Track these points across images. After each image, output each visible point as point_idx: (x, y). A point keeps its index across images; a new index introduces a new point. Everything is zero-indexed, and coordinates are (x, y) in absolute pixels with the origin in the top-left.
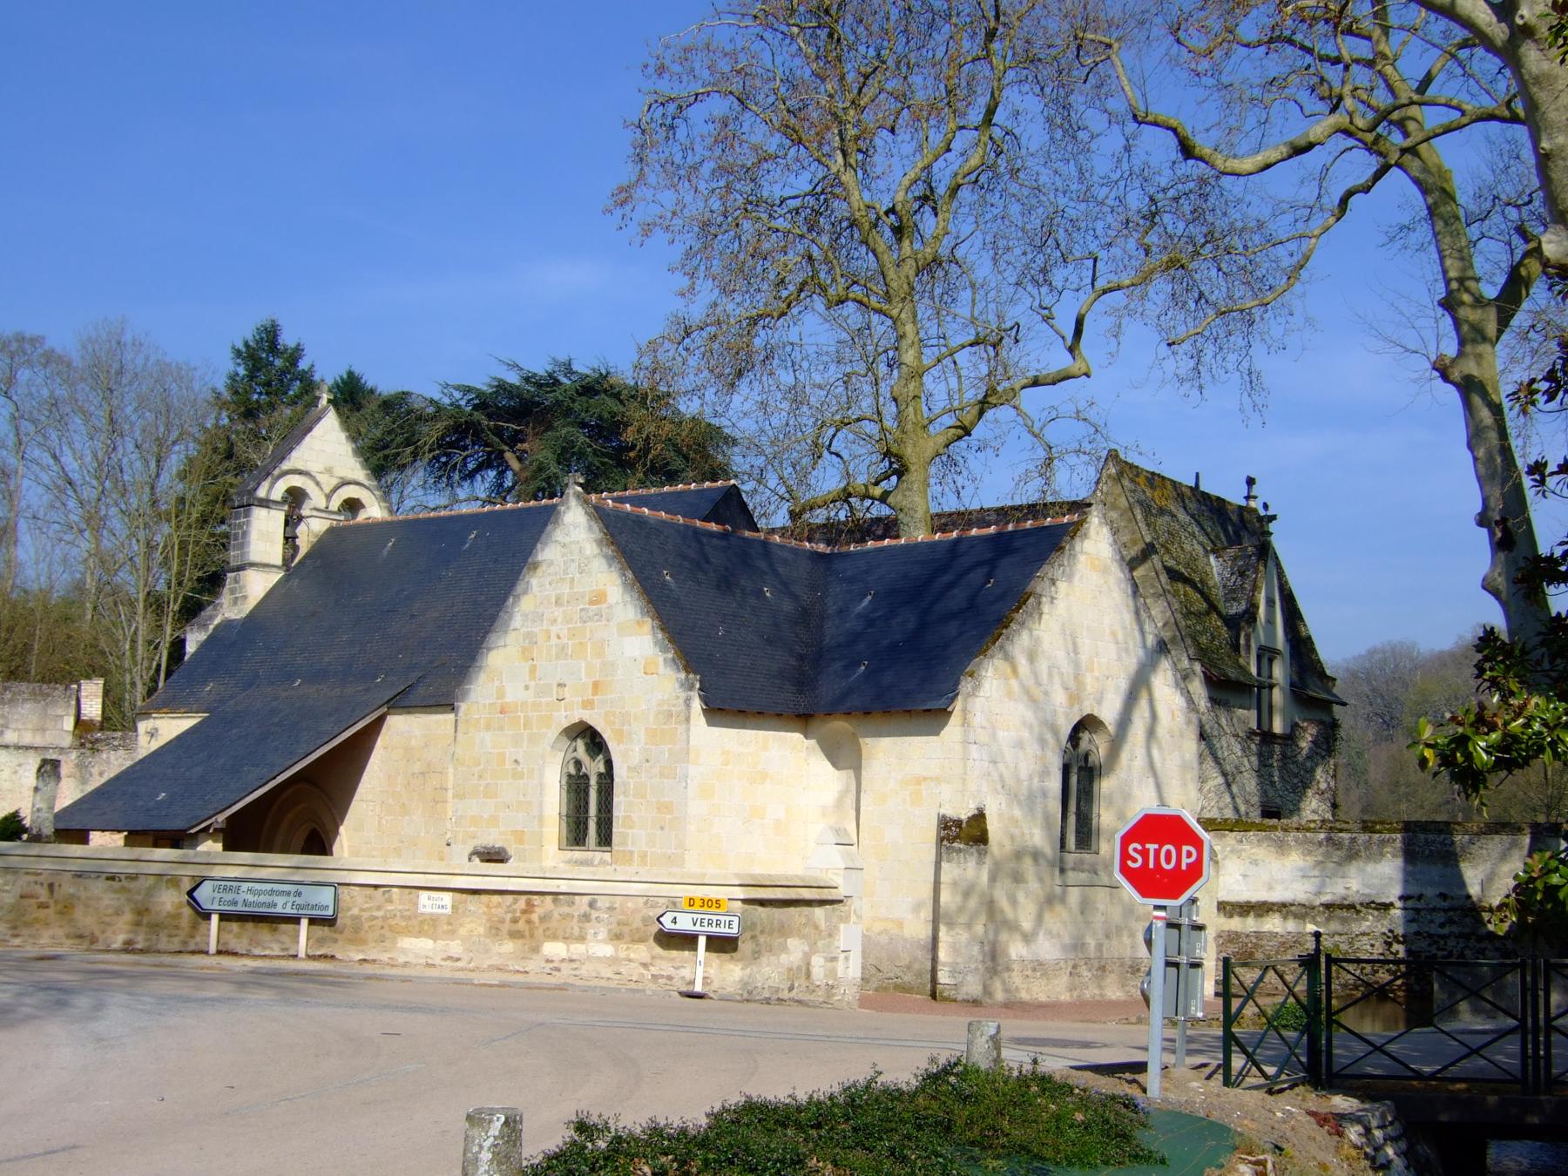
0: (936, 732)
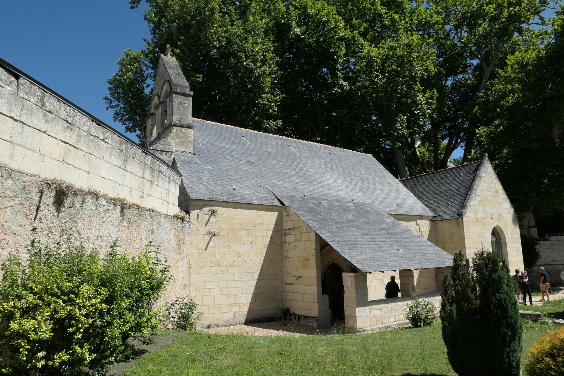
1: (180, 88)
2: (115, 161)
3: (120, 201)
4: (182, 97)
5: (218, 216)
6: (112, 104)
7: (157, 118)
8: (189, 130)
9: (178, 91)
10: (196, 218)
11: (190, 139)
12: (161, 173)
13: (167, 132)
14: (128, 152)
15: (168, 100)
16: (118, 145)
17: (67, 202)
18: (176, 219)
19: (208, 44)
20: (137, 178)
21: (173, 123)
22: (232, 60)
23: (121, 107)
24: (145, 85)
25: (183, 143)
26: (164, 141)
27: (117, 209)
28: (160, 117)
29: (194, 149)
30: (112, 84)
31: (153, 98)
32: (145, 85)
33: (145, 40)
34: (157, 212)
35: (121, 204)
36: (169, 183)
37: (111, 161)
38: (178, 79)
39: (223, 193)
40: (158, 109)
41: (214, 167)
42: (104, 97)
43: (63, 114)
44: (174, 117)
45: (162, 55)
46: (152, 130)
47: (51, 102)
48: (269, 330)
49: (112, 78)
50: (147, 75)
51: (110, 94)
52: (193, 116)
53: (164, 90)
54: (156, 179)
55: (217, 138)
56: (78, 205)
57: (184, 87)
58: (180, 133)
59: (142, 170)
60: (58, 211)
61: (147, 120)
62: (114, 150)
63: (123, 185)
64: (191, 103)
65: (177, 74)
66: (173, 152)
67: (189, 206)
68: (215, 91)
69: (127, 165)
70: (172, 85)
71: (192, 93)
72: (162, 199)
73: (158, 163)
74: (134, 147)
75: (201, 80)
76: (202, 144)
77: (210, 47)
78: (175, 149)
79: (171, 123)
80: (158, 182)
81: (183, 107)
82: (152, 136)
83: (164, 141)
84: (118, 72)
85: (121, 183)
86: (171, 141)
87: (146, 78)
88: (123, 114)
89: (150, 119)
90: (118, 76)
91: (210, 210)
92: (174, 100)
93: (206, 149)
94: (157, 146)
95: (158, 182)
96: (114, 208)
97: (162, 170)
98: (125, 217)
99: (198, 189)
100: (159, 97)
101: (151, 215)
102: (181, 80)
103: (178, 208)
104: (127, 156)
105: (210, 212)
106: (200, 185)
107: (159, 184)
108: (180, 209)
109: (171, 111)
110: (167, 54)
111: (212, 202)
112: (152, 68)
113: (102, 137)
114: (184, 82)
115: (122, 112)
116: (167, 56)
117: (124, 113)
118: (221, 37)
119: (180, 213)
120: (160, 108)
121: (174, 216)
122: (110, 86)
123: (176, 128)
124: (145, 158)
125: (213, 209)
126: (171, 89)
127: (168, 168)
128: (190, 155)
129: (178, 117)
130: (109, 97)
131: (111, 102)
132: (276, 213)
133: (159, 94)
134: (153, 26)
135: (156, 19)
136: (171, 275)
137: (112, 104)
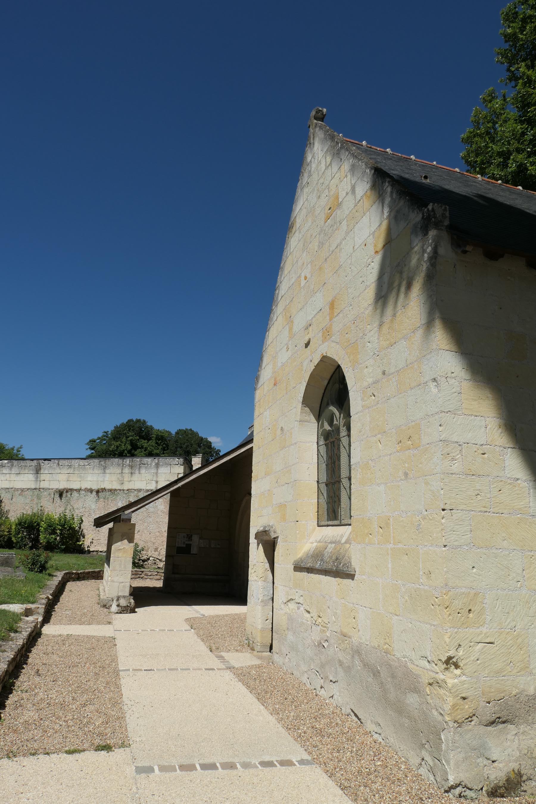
0: (306, 401)
17: (64, 495)
37: (94, 472)
43: (67, 464)
47: (62, 462)
48: (100, 516)
56: (69, 496)
60: (61, 499)
113: (87, 464)
132: (194, 469)
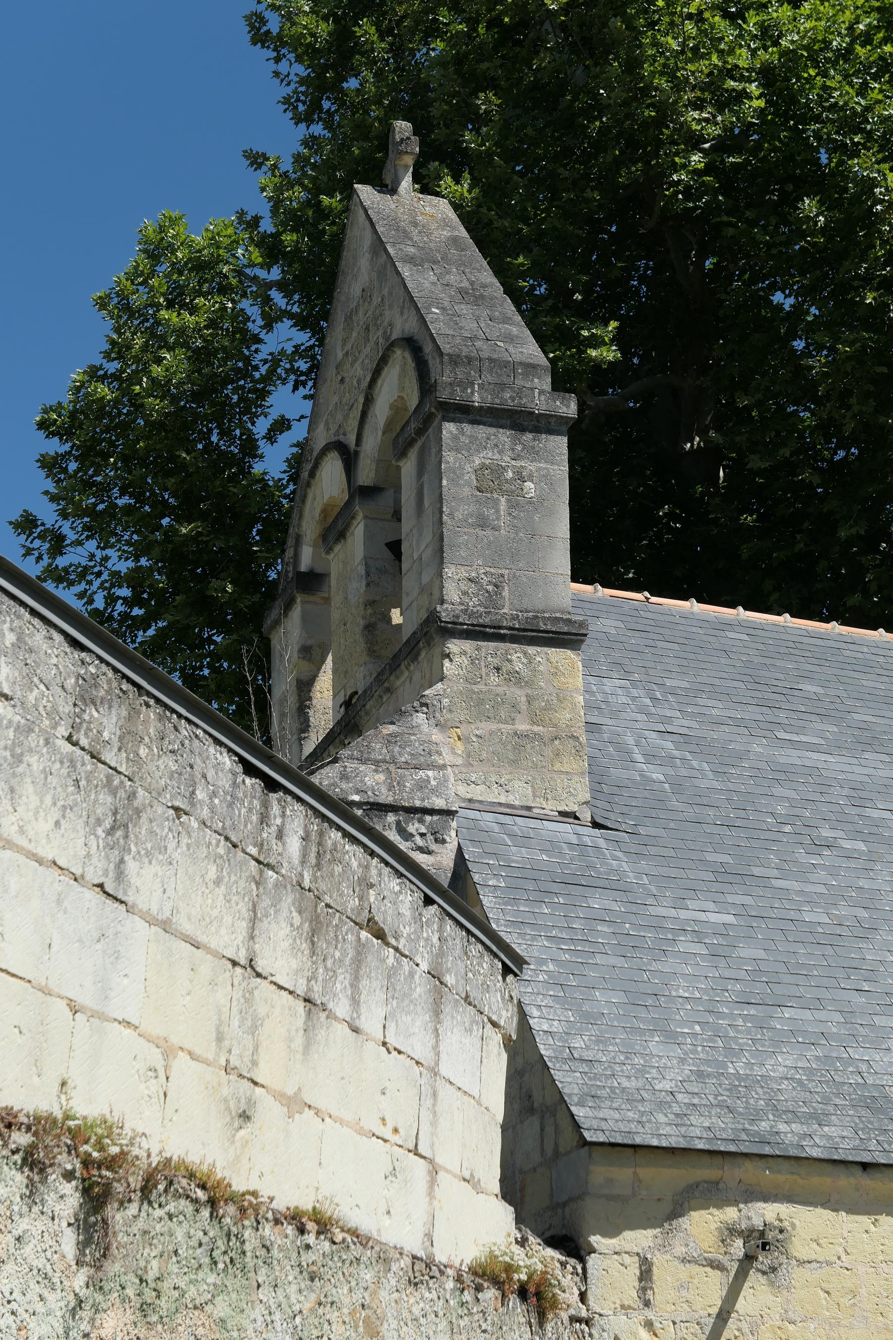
1: (487, 377)
2: (44, 826)
3: (78, 1135)
4: (504, 436)
5: (798, 1275)
6: (62, 562)
7: (337, 600)
8: (556, 654)
9: (477, 399)
10: (631, 1295)
11: (564, 716)
12: (380, 935)
13: (402, 681)
14: (137, 760)
15: (408, 467)
16: (66, 708)
18: (490, 1294)
19: (646, 124)
20: (207, 965)
21: (445, 613)
22: (809, 206)
23: (115, 574)
24: (261, 427)
25: (518, 749)
26: (390, 740)
27: (51, 1198)
28: (357, 588)
29: (596, 791)
30: (65, 433)
31: (312, 474)
32: (261, 427)
33: (256, 160)
34: (354, 1233)
35: (87, 1163)
36: (437, 1013)
38: (469, 326)
39: (826, 1101)
40: (342, 536)
41: (742, 912)
42: (16, 516)
44: (449, 571)
45: (365, 192)
46: (305, 687)
49: (66, 398)
50: (275, 361)
51: (54, 498)
52: (576, 577)
53: (381, 411)
54: (343, 980)
55: (752, 713)
57: (511, 367)
58: (494, 679)
59: (243, 908)
61: (277, 623)
62: (33, 740)
63: (101, 1016)
64: (561, 471)
65: (462, 292)
66: (449, 813)
67: (580, 1197)
68: (703, 434)
69: (131, 866)
70: (433, 363)
71: (569, 408)
72: (387, 1133)
73: (354, 855)
74: (185, 729)
75: (610, 354)
76: (650, 757)
77: (659, 144)
78: (462, 790)
79: (432, 618)
80: (355, 1002)
81: (513, 505)
82: (304, 726)
83: (390, 740)
84: (98, 360)
85: (84, 999)
86: (437, 736)
87: (268, 379)
88: (125, 616)
89: (296, 613)
90: (103, 379)
91: (732, 1231)
92: (449, 457)
93: (677, 786)
94: (344, 777)
95: (355, 1002)
96: (32, 1195)
97: (385, 917)
98: (113, 1267)
99: (641, 1072)
100: (350, 459)
101: (308, 1257)
102: (495, 330)
103: (504, 1214)
104: (132, 796)
105: (738, 1247)
106: (655, 1044)
107: (364, 1023)
108: (520, 1220)
109: (428, 536)
110: (397, 182)
111: (748, 1164)
112: (301, 323)
114: (509, 338)
115: (120, 607)
116: (393, 191)
117: (137, 611)
118: (732, 72)
119: (516, 1248)
120: (358, 531)
121: (473, 1271)
122: (55, 446)
123: (468, 645)
124: (264, 819)
125: (758, 1223)
126: (426, 385)
127: (428, 901)
128: (566, 829)
129: (479, 569)
130: (47, 513)
131: (58, 544)
133: (351, 440)
134: (300, 70)
135: (324, 29)
136: (157, 1152)
137: (62, 562)
